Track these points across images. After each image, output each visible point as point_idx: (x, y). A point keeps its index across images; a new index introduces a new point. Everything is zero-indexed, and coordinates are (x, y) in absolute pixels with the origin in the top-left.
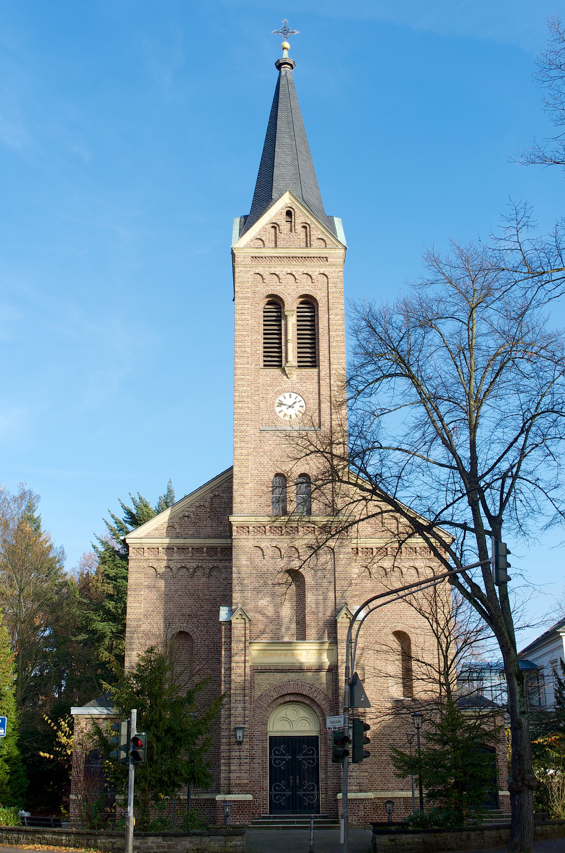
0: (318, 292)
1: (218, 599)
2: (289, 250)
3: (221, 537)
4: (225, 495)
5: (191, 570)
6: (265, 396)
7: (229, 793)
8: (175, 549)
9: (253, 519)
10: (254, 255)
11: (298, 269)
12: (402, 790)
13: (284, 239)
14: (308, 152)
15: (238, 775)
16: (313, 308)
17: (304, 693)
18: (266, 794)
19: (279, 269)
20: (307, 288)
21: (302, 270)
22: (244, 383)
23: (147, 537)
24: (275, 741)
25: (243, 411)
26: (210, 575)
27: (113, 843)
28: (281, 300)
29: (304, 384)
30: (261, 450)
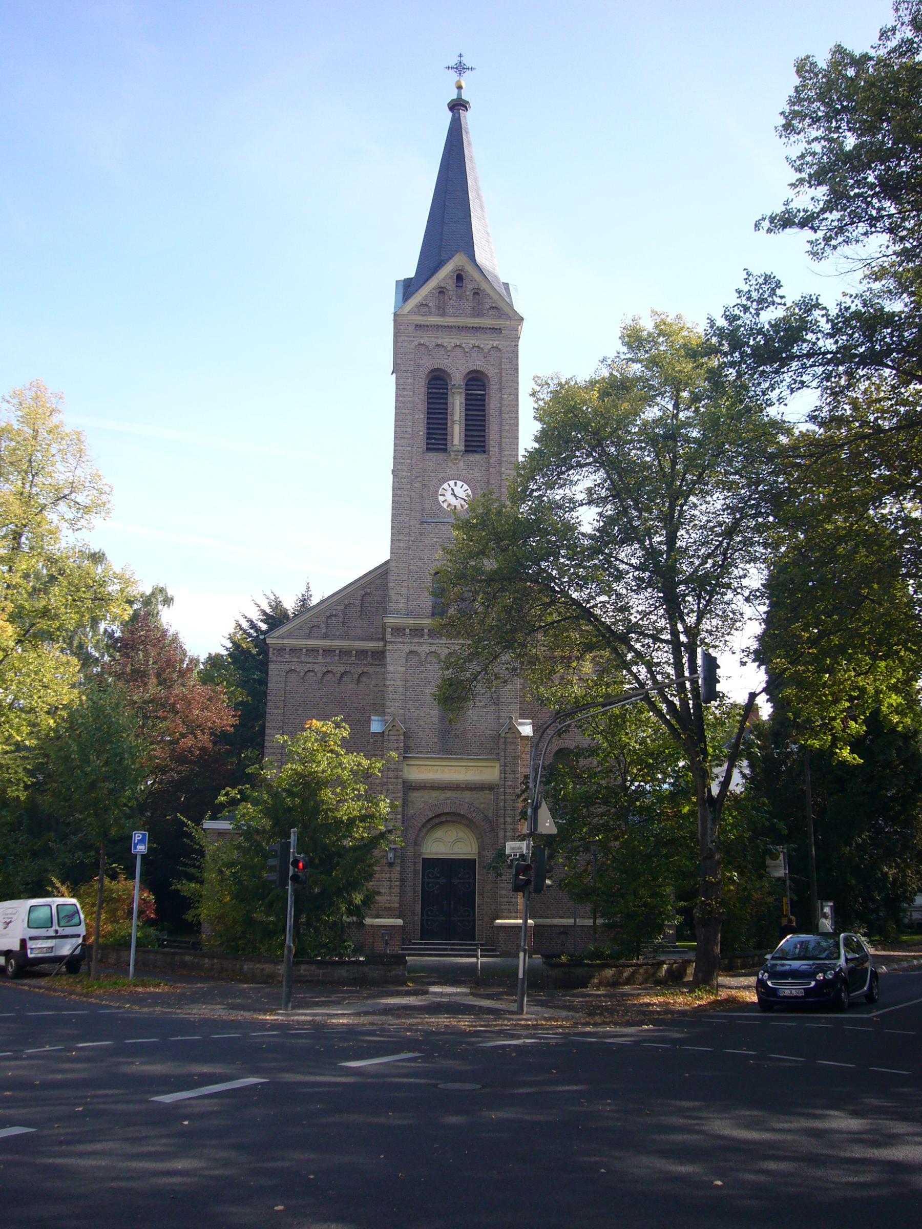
0: (490, 367)
1: (367, 708)
2: (459, 320)
3: (372, 639)
4: (377, 593)
5: (302, 674)
6: (427, 483)
7: (378, 917)
8: (304, 650)
9: (411, 621)
10: (419, 323)
11: (469, 341)
12: (562, 917)
13: (453, 306)
14: (482, 208)
15: (388, 898)
16: (484, 385)
17: (462, 812)
18: (418, 919)
19: (447, 340)
20: (477, 363)
21: (473, 342)
22: (404, 467)
23: (289, 635)
24: (429, 863)
25: (402, 499)
26: (358, 681)
27: (263, 969)
28: (482, 373)
29: (471, 472)
30: (420, 544)
